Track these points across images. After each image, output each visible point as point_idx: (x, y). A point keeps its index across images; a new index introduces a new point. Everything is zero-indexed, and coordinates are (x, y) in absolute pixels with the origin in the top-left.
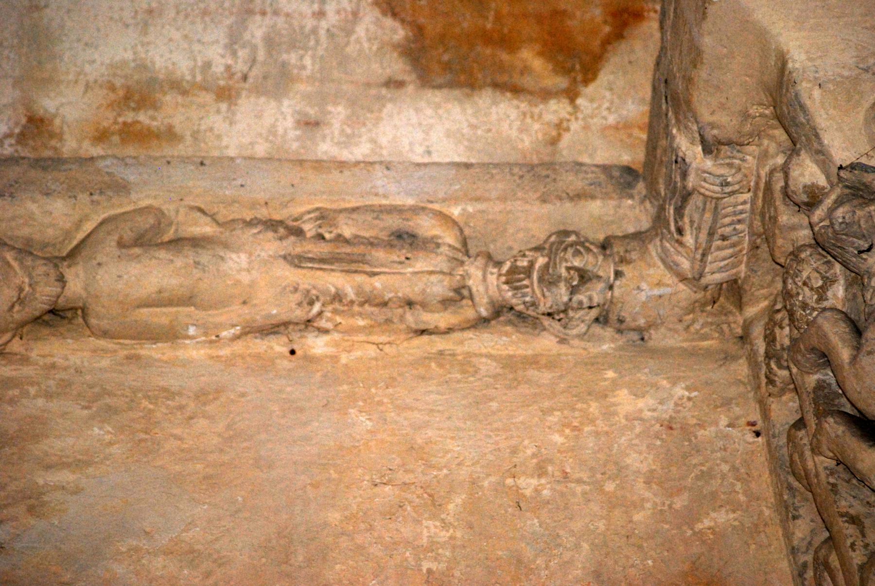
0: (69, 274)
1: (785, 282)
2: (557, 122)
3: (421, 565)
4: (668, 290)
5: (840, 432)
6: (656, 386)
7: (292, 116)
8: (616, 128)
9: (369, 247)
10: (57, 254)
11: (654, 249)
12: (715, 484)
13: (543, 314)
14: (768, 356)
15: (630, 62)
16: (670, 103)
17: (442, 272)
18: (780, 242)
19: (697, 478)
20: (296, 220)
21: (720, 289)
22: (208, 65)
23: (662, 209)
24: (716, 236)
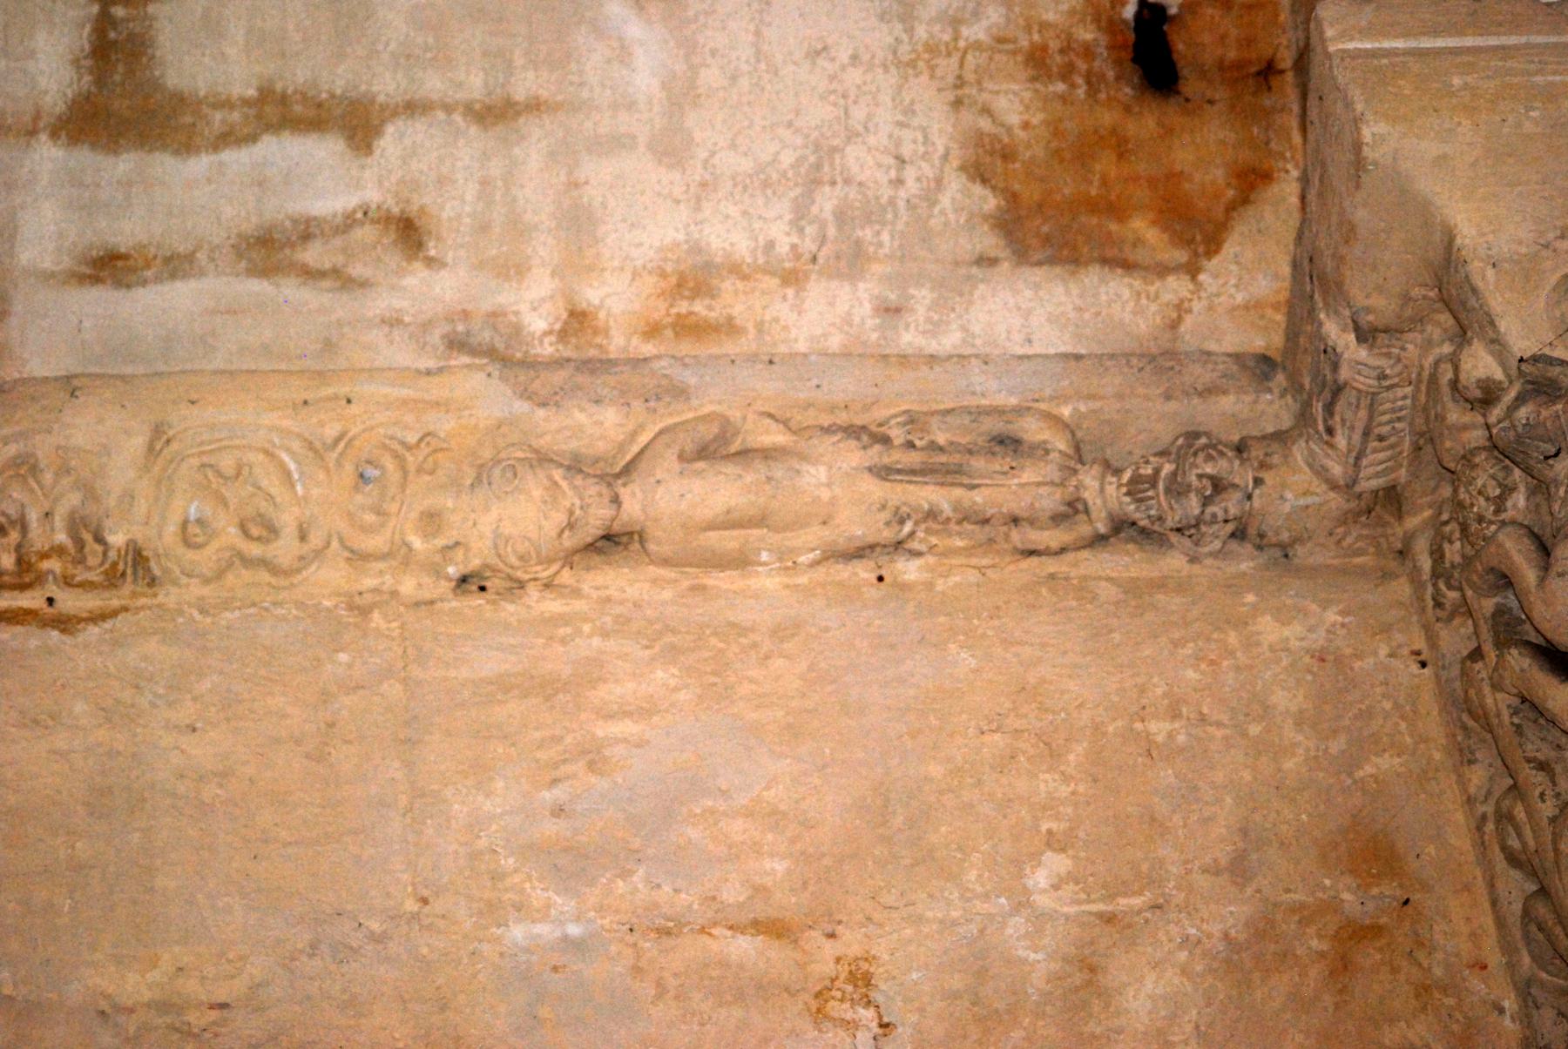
0: (624, 493)
1: (1455, 491)
2: (1176, 302)
3: (1039, 826)
4: (1317, 499)
5: (1525, 666)
6: (1306, 613)
7: (870, 302)
8: (1247, 307)
9: (968, 456)
10: (608, 470)
11: (1299, 452)
12: (1376, 724)
13: (1172, 530)
14: (1435, 575)
15: (1259, 231)
16: (1316, 283)
17: (1052, 483)
18: (1448, 444)
19: (1356, 717)
20: (880, 425)
21: (1376, 496)
22: (770, 245)
23: (1307, 405)
24: (1372, 437)
